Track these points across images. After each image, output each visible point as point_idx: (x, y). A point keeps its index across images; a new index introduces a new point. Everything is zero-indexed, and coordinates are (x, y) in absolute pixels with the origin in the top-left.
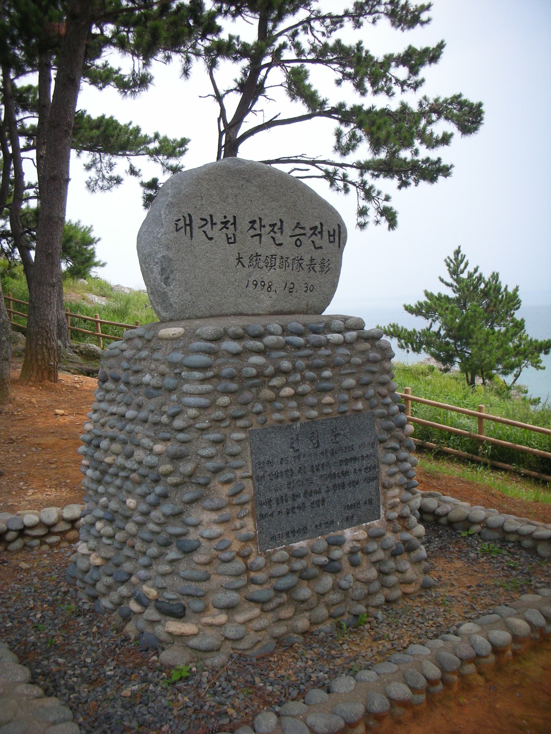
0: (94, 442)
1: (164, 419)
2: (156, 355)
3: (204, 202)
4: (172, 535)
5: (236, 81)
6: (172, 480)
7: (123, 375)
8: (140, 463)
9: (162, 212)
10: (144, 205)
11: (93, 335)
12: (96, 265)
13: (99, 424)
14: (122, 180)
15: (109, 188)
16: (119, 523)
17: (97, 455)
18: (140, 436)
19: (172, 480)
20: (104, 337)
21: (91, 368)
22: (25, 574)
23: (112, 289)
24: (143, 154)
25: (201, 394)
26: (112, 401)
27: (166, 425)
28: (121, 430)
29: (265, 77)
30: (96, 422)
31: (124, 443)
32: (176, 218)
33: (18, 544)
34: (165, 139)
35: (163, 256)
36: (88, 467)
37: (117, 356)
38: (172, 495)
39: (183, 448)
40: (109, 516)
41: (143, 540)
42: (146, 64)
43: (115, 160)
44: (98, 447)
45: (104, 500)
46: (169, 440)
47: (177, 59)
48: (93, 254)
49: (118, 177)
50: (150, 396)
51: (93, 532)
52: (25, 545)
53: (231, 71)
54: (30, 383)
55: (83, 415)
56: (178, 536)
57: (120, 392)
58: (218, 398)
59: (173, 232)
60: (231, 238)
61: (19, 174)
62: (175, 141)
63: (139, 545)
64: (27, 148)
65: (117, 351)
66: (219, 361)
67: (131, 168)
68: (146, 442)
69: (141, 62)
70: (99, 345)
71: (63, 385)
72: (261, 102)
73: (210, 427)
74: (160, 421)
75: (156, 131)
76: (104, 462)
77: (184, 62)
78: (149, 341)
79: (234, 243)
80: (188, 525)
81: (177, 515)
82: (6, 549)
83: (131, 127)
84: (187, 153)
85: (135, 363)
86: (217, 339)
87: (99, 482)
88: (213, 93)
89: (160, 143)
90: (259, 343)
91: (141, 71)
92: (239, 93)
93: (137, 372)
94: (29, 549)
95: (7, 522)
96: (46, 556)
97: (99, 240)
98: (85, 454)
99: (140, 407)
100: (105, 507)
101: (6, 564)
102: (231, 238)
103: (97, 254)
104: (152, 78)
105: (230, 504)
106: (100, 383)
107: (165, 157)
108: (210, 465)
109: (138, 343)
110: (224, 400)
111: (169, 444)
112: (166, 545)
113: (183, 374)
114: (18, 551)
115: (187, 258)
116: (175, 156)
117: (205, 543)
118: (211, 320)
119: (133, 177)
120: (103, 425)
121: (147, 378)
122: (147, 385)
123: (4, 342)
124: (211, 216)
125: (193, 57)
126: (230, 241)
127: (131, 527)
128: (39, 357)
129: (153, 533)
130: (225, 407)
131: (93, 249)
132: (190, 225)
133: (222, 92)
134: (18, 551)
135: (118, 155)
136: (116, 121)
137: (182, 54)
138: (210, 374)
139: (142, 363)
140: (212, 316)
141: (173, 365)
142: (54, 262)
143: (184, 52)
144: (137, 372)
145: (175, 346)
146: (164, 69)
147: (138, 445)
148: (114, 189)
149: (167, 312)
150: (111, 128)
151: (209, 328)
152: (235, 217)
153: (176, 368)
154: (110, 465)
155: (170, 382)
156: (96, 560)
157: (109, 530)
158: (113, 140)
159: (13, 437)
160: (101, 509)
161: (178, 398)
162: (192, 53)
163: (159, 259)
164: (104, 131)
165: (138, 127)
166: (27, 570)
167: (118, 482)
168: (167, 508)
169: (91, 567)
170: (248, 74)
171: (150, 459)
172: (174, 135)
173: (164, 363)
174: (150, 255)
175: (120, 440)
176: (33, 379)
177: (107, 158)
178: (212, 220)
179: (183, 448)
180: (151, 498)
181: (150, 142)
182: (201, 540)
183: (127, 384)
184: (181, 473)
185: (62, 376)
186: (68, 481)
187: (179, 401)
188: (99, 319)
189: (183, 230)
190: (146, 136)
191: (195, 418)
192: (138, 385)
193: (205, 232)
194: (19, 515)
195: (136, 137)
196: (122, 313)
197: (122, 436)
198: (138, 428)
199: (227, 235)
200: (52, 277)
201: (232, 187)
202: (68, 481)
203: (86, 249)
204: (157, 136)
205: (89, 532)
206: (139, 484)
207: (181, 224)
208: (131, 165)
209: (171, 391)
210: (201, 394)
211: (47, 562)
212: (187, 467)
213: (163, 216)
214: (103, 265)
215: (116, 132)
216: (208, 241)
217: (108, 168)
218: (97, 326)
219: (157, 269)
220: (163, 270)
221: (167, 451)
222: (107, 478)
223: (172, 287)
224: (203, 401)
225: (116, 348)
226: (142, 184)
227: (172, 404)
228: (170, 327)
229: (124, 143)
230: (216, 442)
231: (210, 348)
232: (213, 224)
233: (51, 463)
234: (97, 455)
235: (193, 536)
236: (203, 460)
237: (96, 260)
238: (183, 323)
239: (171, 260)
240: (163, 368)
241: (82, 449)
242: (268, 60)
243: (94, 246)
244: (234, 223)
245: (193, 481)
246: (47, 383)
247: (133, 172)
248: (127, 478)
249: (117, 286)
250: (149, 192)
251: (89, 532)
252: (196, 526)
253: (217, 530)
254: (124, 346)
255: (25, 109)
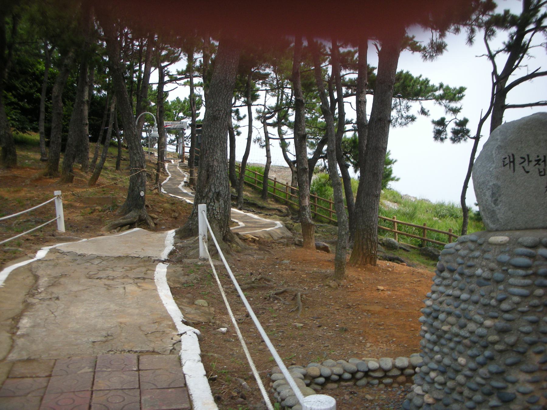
0: (434, 314)
1: (493, 302)
2: (487, 255)
3: (523, 145)
4: (494, 388)
5: (504, 43)
6: (498, 347)
7: (459, 268)
8: (472, 333)
9: (493, 152)
10: (434, 137)
11: (391, 231)
12: (392, 179)
13: (437, 302)
14: (415, 118)
15: (406, 124)
16: (450, 374)
17: (436, 324)
18: (472, 313)
19: (498, 347)
20: (399, 233)
21: (392, 256)
22: (370, 403)
23: (402, 197)
24: (431, 99)
25: (523, 286)
26: (447, 286)
27: (494, 307)
28: (456, 307)
29: (530, 40)
30: (434, 300)
31: (458, 317)
32: (504, 157)
33: (363, 382)
34: (448, 88)
35: (494, 184)
36: (426, 332)
37: (453, 254)
38: (497, 358)
39: (508, 325)
40: (442, 369)
41: (470, 389)
42: (442, 35)
43: (411, 103)
44: (436, 318)
45: (438, 357)
46: (496, 318)
47: (464, 31)
48: (390, 172)
49: (413, 116)
50: (480, 285)
51: (427, 378)
52: (368, 383)
53: (502, 37)
54: (357, 265)
55: (397, 291)
56: (498, 389)
57: (455, 280)
58: (535, 290)
59: (501, 167)
60: (541, 172)
61: (342, 113)
62: (455, 89)
63: (466, 392)
64: (347, 95)
65: (452, 250)
66: (537, 263)
67: (422, 109)
68: (477, 317)
69: (438, 34)
70: (395, 239)
71: (380, 269)
72: (525, 60)
73: (529, 311)
74: (489, 304)
75: (440, 82)
76: (440, 329)
77: (469, 32)
78: (481, 245)
79: (544, 175)
80: (507, 381)
81: (500, 374)
82: (355, 384)
83: (421, 79)
84: (464, 98)
85: (469, 260)
86: (534, 246)
87: (435, 343)
88: (487, 53)
89: (444, 90)
90: (16, 173)
91: (438, 40)
92: (507, 53)
93: (470, 267)
94: (371, 386)
95: (357, 365)
96: (383, 392)
97: (396, 161)
98: (424, 323)
99: (472, 292)
100: (439, 362)
101: (356, 395)
102: (541, 172)
103: (393, 172)
104: (446, 45)
105: (540, 370)
106: (438, 272)
107: (448, 101)
108: (528, 339)
109: (472, 246)
110: (540, 292)
111: (496, 321)
112: (490, 394)
113: (510, 270)
114: (364, 386)
115: (510, 186)
116: (455, 100)
117: (519, 396)
118: (528, 232)
119: (423, 116)
120: (441, 303)
121: (479, 271)
122: (479, 277)
123: (343, 235)
124: (528, 156)
125: (476, 28)
126: (542, 173)
127: (460, 378)
128: (365, 247)
129: (479, 384)
130: (540, 297)
131: (391, 168)
132: (513, 162)
133: (493, 53)
134: (364, 386)
135: (412, 100)
136: (410, 75)
137: (468, 27)
138: (530, 272)
139: (475, 260)
140: (526, 229)
141: (501, 263)
142: (378, 180)
143: (469, 25)
144: (470, 267)
145: (503, 250)
146: (455, 40)
147: (470, 320)
148: (409, 124)
149: (494, 224)
150: (408, 81)
151: (529, 238)
152: (545, 157)
153: (504, 266)
154: (445, 332)
155: (498, 275)
156: (428, 399)
157: (441, 379)
158: (409, 89)
159: (350, 304)
160: (435, 363)
161: (505, 287)
162: (475, 25)
163: (490, 186)
164: (403, 83)
165: (426, 79)
166: (371, 401)
167: (452, 345)
168: (493, 368)
169: (424, 404)
170: (514, 38)
171: (481, 331)
172: (454, 85)
173: (493, 262)
174: (483, 183)
175: (456, 315)
176: (359, 262)
177: (405, 102)
178: (528, 159)
179: (508, 325)
180: (480, 359)
181: (436, 90)
182: (517, 393)
183: (461, 274)
184: (505, 343)
185: (378, 262)
186: (394, 339)
187: (505, 290)
188: (395, 220)
189: (508, 166)
190: (433, 86)
191: (518, 304)
192: (470, 276)
193: (523, 167)
194: (364, 360)
195: (426, 87)
196: (412, 216)
197: (457, 312)
198: (471, 307)
199: (539, 170)
200: (376, 190)
201: (543, 134)
202: (394, 339)
203: (386, 168)
204: (441, 86)
205: (423, 379)
206: (469, 347)
207: (507, 161)
208: (422, 107)
209: (498, 282)
210: (523, 286)
211: (385, 397)
212: (511, 339)
213: (494, 155)
214: (397, 180)
215: (411, 84)
216: (525, 174)
217: (405, 110)
218: (394, 226)
219: (488, 194)
220: (493, 194)
221: (495, 325)
222: (443, 341)
223: (499, 207)
224: (525, 291)
225: (451, 248)
226: (433, 122)
227: (499, 292)
228: (497, 236)
229: (418, 91)
230: (532, 323)
231: (530, 253)
232: (529, 161)
233: (380, 325)
234: (436, 324)
235: (511, 390)
236: (522, 335)
237: (392, 176)
238: (507, 233)
239: (499, 187)
240: (493, 265)
241: (422, 318)
242: (532, 26)
243: (392, 165)
244: (544, 161)
245: (515, 349)
246: (369, 266)
247: (423, 112)
248: (459, 343)
249: (406, 195)
250: (438, 128)
251: (423, 379)
252: (513, 383)
253: (529, 387)
254: (459, 247)
255: (346, 68)
